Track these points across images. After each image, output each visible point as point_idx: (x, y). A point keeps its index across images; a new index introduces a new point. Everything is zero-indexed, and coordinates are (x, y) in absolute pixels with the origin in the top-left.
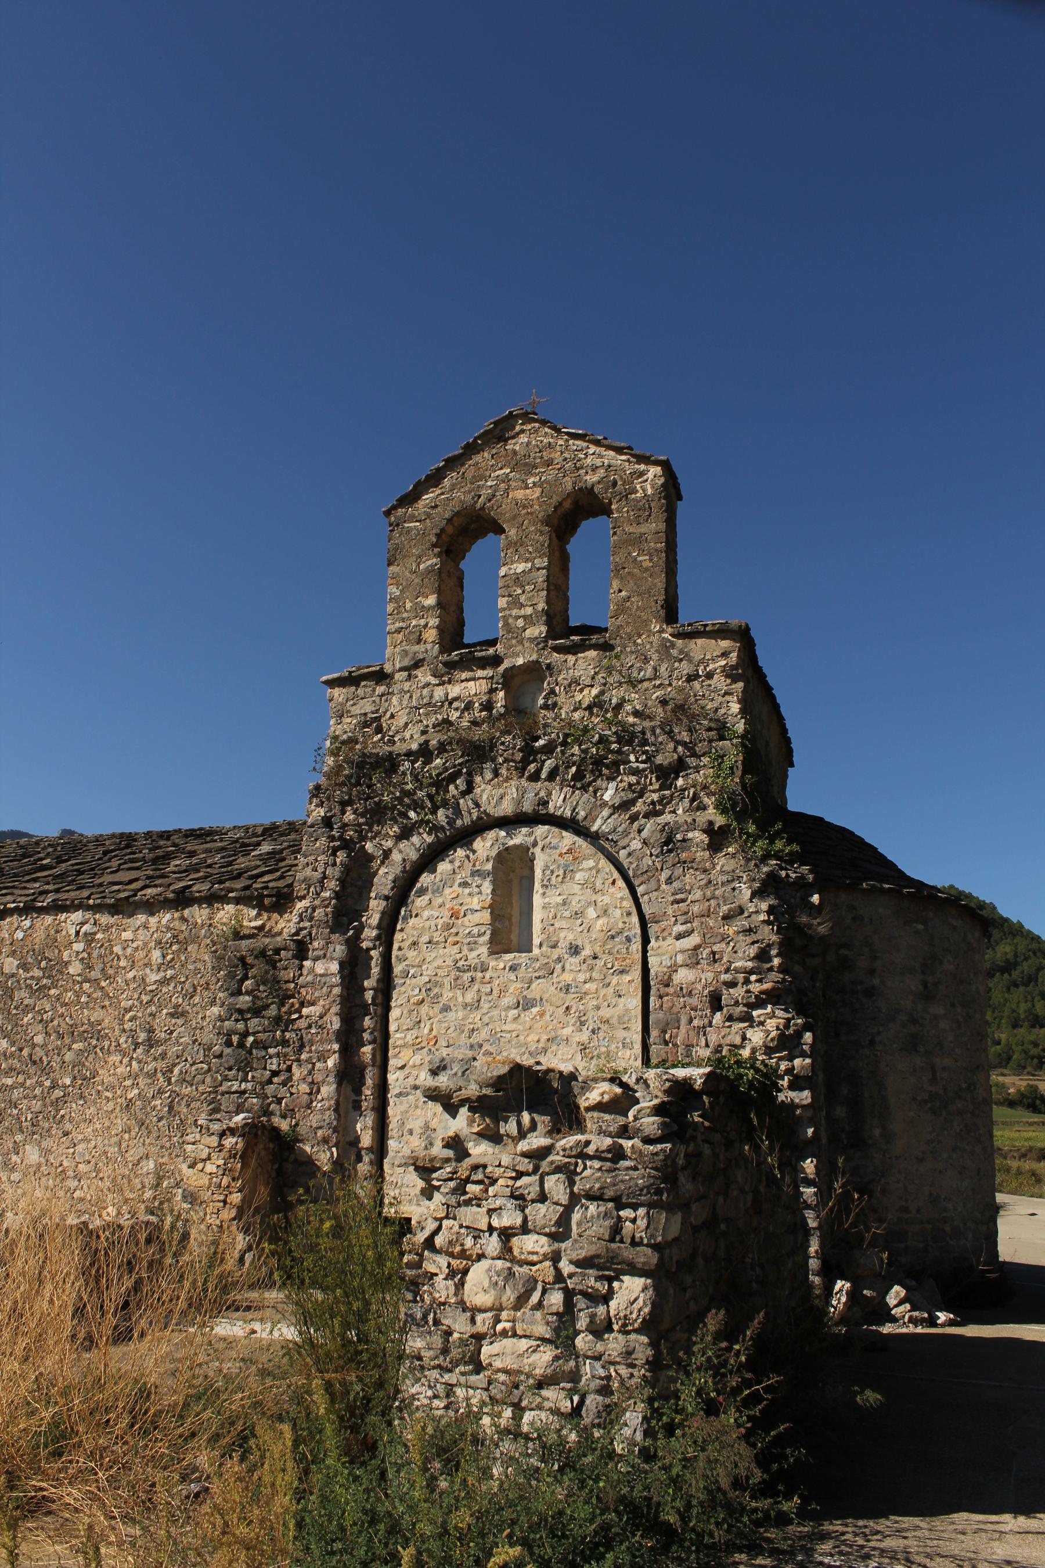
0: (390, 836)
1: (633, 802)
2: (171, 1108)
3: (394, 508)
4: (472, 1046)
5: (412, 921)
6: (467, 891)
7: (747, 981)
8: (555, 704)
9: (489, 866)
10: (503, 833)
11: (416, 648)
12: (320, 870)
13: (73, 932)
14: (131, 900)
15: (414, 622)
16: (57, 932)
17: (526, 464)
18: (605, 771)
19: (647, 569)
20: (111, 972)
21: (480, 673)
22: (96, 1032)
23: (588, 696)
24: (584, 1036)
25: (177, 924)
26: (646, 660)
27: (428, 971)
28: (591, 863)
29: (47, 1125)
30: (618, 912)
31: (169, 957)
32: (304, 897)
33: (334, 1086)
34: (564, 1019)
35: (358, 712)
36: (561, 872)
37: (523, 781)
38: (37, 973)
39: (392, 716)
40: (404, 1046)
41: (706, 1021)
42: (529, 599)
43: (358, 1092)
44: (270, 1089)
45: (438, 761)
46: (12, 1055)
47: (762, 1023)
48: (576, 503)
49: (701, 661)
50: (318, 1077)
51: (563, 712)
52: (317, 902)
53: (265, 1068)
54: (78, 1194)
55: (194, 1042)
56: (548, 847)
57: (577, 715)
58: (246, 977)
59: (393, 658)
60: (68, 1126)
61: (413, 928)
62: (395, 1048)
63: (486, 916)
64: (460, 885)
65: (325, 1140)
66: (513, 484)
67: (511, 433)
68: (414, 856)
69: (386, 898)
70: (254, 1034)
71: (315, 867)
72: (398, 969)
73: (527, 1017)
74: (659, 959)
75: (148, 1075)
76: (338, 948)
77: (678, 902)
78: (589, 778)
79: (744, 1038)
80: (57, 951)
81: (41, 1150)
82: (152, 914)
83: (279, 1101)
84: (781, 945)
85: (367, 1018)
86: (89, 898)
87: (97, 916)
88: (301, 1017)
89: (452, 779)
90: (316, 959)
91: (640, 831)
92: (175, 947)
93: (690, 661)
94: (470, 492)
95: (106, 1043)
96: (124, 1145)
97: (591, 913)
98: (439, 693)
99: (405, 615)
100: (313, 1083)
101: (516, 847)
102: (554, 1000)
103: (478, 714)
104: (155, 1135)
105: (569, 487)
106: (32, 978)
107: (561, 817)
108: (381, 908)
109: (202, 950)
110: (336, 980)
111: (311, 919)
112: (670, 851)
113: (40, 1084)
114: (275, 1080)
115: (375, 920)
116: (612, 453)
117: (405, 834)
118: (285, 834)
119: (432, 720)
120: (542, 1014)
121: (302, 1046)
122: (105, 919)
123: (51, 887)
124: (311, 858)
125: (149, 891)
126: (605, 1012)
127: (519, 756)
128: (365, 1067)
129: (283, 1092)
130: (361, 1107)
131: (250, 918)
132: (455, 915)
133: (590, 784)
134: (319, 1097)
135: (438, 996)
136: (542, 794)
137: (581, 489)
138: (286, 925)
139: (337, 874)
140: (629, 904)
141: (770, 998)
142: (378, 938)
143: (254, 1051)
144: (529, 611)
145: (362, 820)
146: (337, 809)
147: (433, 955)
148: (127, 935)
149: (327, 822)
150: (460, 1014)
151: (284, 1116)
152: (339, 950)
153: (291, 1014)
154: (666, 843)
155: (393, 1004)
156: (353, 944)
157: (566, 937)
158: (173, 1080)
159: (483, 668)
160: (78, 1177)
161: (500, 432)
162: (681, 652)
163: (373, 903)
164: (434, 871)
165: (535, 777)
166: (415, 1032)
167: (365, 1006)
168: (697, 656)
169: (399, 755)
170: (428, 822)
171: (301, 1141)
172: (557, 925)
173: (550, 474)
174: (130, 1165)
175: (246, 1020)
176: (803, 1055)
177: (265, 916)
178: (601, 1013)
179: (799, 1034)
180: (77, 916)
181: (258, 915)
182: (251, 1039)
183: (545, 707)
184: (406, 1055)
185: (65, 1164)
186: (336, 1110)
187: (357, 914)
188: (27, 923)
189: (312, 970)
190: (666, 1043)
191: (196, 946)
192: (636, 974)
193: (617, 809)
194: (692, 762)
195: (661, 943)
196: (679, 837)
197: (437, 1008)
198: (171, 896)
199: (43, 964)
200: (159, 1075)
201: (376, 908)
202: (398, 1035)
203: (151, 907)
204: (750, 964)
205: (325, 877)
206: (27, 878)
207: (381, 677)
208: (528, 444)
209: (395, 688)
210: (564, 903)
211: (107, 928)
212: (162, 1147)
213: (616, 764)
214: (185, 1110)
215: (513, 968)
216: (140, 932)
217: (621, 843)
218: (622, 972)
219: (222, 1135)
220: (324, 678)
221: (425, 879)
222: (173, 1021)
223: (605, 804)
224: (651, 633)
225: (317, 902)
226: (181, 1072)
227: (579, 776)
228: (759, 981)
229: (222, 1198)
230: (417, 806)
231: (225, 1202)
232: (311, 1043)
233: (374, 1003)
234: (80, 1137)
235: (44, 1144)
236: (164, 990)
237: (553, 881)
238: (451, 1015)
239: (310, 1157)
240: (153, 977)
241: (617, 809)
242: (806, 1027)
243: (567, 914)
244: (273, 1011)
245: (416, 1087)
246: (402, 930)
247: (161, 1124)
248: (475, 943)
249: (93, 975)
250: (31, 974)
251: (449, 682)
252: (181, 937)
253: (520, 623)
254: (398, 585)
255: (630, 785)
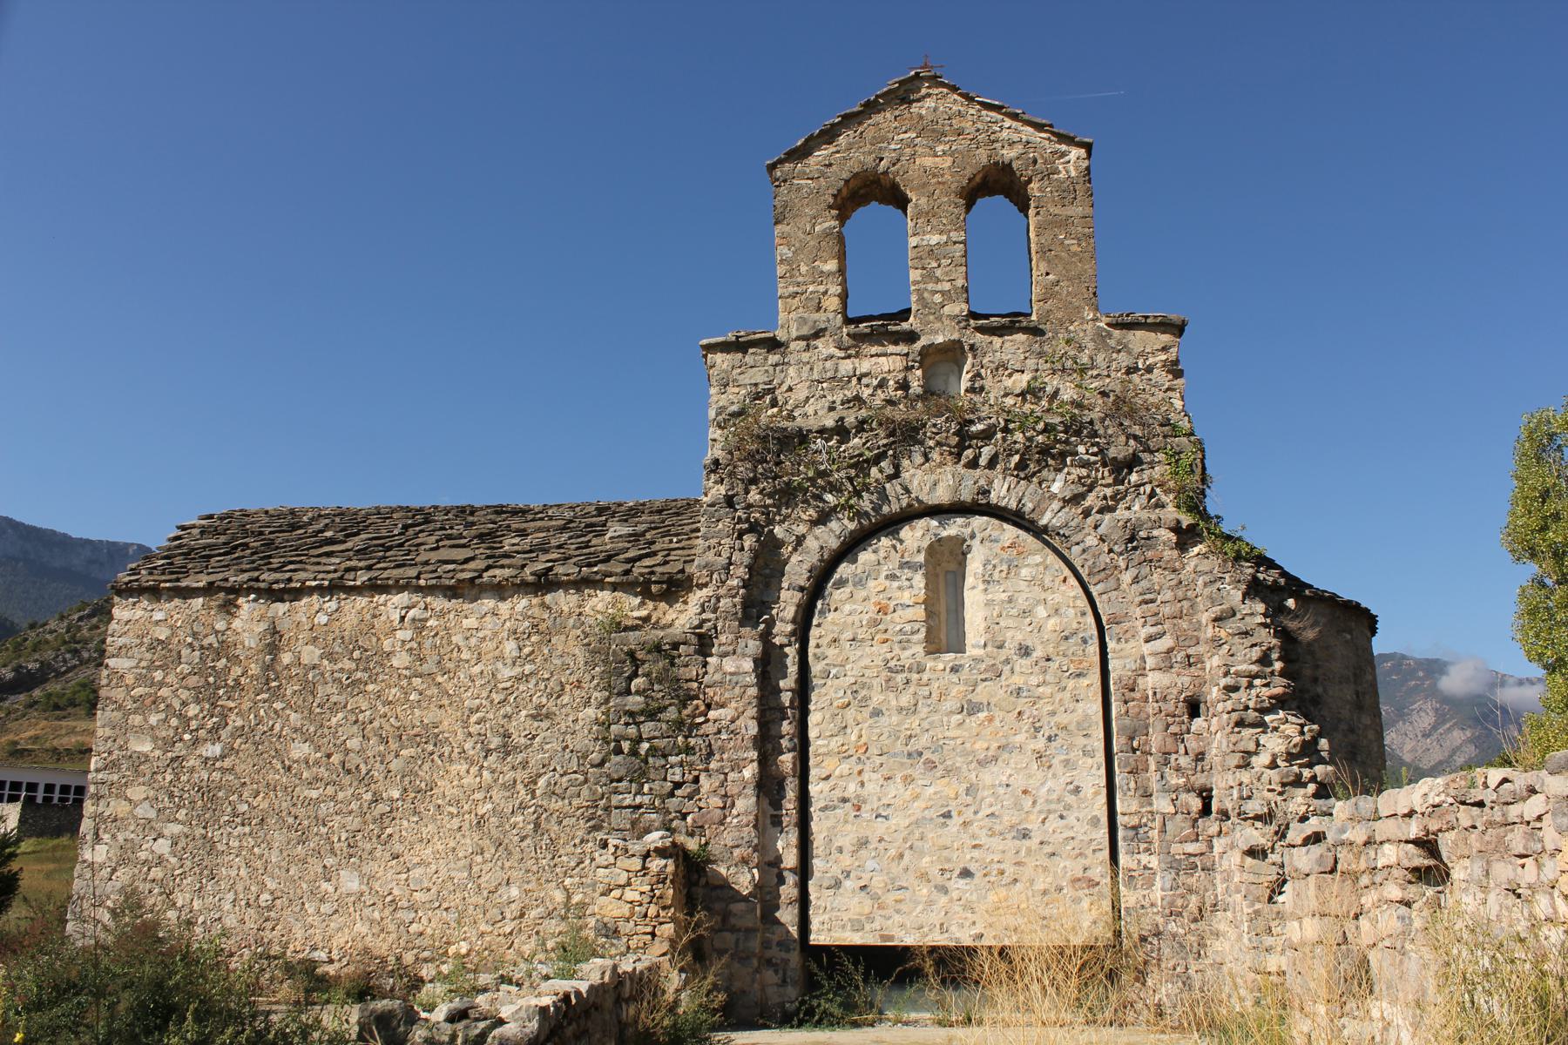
0: (803, 521)
1: (1083, 496)
2: (537, 825)
3: (781, 161)
4: (910, 755)
5: (831, 616)
6: (896, 584)
7: (1250, 686)
8: (982, 388)
9: (921, 558)
10: (934, 523)
11: (816, 316)
12: (725, 554)
13: (396, 617)
14: (478, 581)
15: (811, 288)
16: (374, 616)
17: (934, 131)
18: (1051, 462)
19: (1075, 254)
20: (451, 665)
21: (891, 349)
22: (430, 736)
23: (1022, 381)
24: (1040, 743)
25: (536, 611)
26: (1081, 349)
27: (852, 671)
28: (1038, 559)
29: (368, 846)
30: (1072, 611)
31: (527, 650)
32: (705, 585)
33: (754, 799)
34: (1016, 725)
35: (747, 381)
36: (1005, 567)
37: (959, 467)
38: (348, 665)
39: (790, 389)
40: (827, 754)
41: (1184, 727)
42: (947, 274)
43: (778, 806)
44: (672, 803)
45: (856, 440)
46: (317, 762)
47: (1276, 729)
48: (985, 178)
49: (1140, 354)
50: (732, 789)
51: (992, 396)
52: (722, 591)
53: (665, 779)
54: (414, 928)
55: (564, 749)
56: (988, 542)
57: (1010, 401)
58: (635, 675)
59: (787, 325)
60: (398, 848)
61: (833, 623)
62: (816, 756)
63: (920, 613)
64: (887, 577)
65: (744, 861)
66: (920, 150)
67: (916, 96)
68: (834, 544)
69: (802, 589)
70: (649, 740)
71: (716, 551)
72: (816, 668)
73: (972, 722)
74: (1122, 662)
75: (505, 786)
76: (751, 643)
77: (1146, 602)
78: (1032, 467)
79: (1258, 744)
80: (374, 639)
81: (362, 876)
82: (503, 599)
83: (684, 817)
84: (1282, 648)
85: (785, 723)
86: (418, 578)
87: (429, 599)
88: (707, 721)
89: (877, 460)
90: (724, 655)
91: (1096, 527)
92: (534, 639)
93: (1129, 353)
94: (870, 153)
95: (447, 750)
96: (475, 869)
97: (1041, 612)
98: (846, 367)
99: (800, 279)
100: (726, 795)
101: (950, 538)
102: (1004, 704)
103: (891, 391)
104: (517, 856)
105: (985, 161)
106: (342, 670)
107: (1005, 509)
108: (796, 600)
109: (571, 642)
110: (751, 679)
111: (715, 611)
112: (1135, 548)
113: (358, 798)
114: (678, 792)
115: (790, 612)
116: (1030, 129)
117: (823, 518)
118: (674, 516)
119: (838, 397)
120: (991, 720)
121: (711, 754)
122: (439, 603)
123: (362, 564)
124: (713, 542)
125: (497, 572)
126: (1062, 718)
127: (954, 440)
128: (784, 778)
129: (689, 805)
130: (781, 823)
131: (632, 606)
132: (882, 610)
133: (1034, 474)
134: (734, 812)
135: (866, 699)
136: (982, 482)
137: (996, 163)
138: (682, 617)
139: (747, 561)
140: (1083, 603)
141: (1280, 703)
142: (793, 633)
143: (651, 760)
144: (947, 286)
145: (769, 501)
146: (740, 488)
147: (859, 653)
148: (470, 622)
149: (729, 501)
150: (895, 719)
151: (692, 835)
152: (754, 646)
153: (694, 717)
154: (1131, 540)
155: (812, 707)
156: (766, 637)
157: (1013, 638)
158: (538, 792)
159: (896, 343)
160: (413, 908)
161: (904, 94)
162: (1119, 343)
163: (784, 595)
164: (855, 561)
165: (973, 464)
166: (840, 739)
167: (782, 709)
168: (1137, 349)
169: (809, 431)
170: (851, 507)
171: (714, 862)
172: (1002, 624)
173: (961, 144)
174: (485, 893)
175: (638, 724)
176: (1322, 761)
177: (650, 605)
178: (1056, 719)
179: (1315, 740)
180: (402, 598)
181: (642, 604)
182: (645, 746)
183: (971, 390)
184: (830, 765)
185: (396, 892)
186: (755, 827)
187: (766, 606)
188: (333, 605)
189: (719, 668)
190: (1134, 751)
191: (563, 637)
192: (1095, 677)
193: (1066, 502)
194: (1146, 457)
195: (1123, 645)
196: (1143, 534)
197: (866, 712)
198: (531, 578)
199: (356, 654)
200: (520, 787)
201: (787, 604)
202: (820, 742)
203: (500, 591)
204: (1255, 668)
205: (730, 564)
206: (313, 552)
207: (773, 345)
208: (935, 110)
209: (792, 358)
210: (1010, 601)
211: (442, 614)
212: (528, 871)
213: (1063, 455)
214: (556, 828)
215: (955, 670)
216: (488, 618)
217: (1074, 539)
218: (1079, 675)
219: (646, 856)
220: (705, 342)
221: (844, 570)
222: (536, 724)
223: (1053, 497)
224: (1084, 321)
225: (722, 591)
226: (549, 784)
227: (1021, 466)
228: (1266, 685)
229: (649, 929)
230: (835, 488)
231: (653, 934)
232: (722, 750)
233: (792, 706)
234: (416, 860)
235: (366, 869)
236: (522, 688)
237: (996, 576)
238: (883, 720)
239: (725, 880)
240: (506, 672)
241: (1066, 502)
242: (1320, 734)
243: (1014, 612)
244: (671, 714)
245: (844, 800)
246: (819, 625)
247: (524, 844)
248: (908, 641)
249: (425, 668)
250: (340, 665)
251: (857, 356)
252: (543, 627)
253: (938, 298)
254: (789, 245)
255: (1080, 478)
